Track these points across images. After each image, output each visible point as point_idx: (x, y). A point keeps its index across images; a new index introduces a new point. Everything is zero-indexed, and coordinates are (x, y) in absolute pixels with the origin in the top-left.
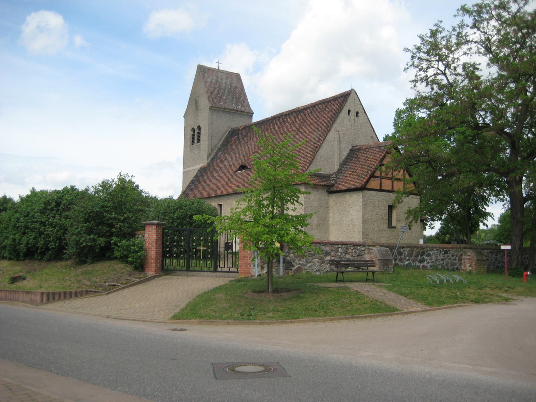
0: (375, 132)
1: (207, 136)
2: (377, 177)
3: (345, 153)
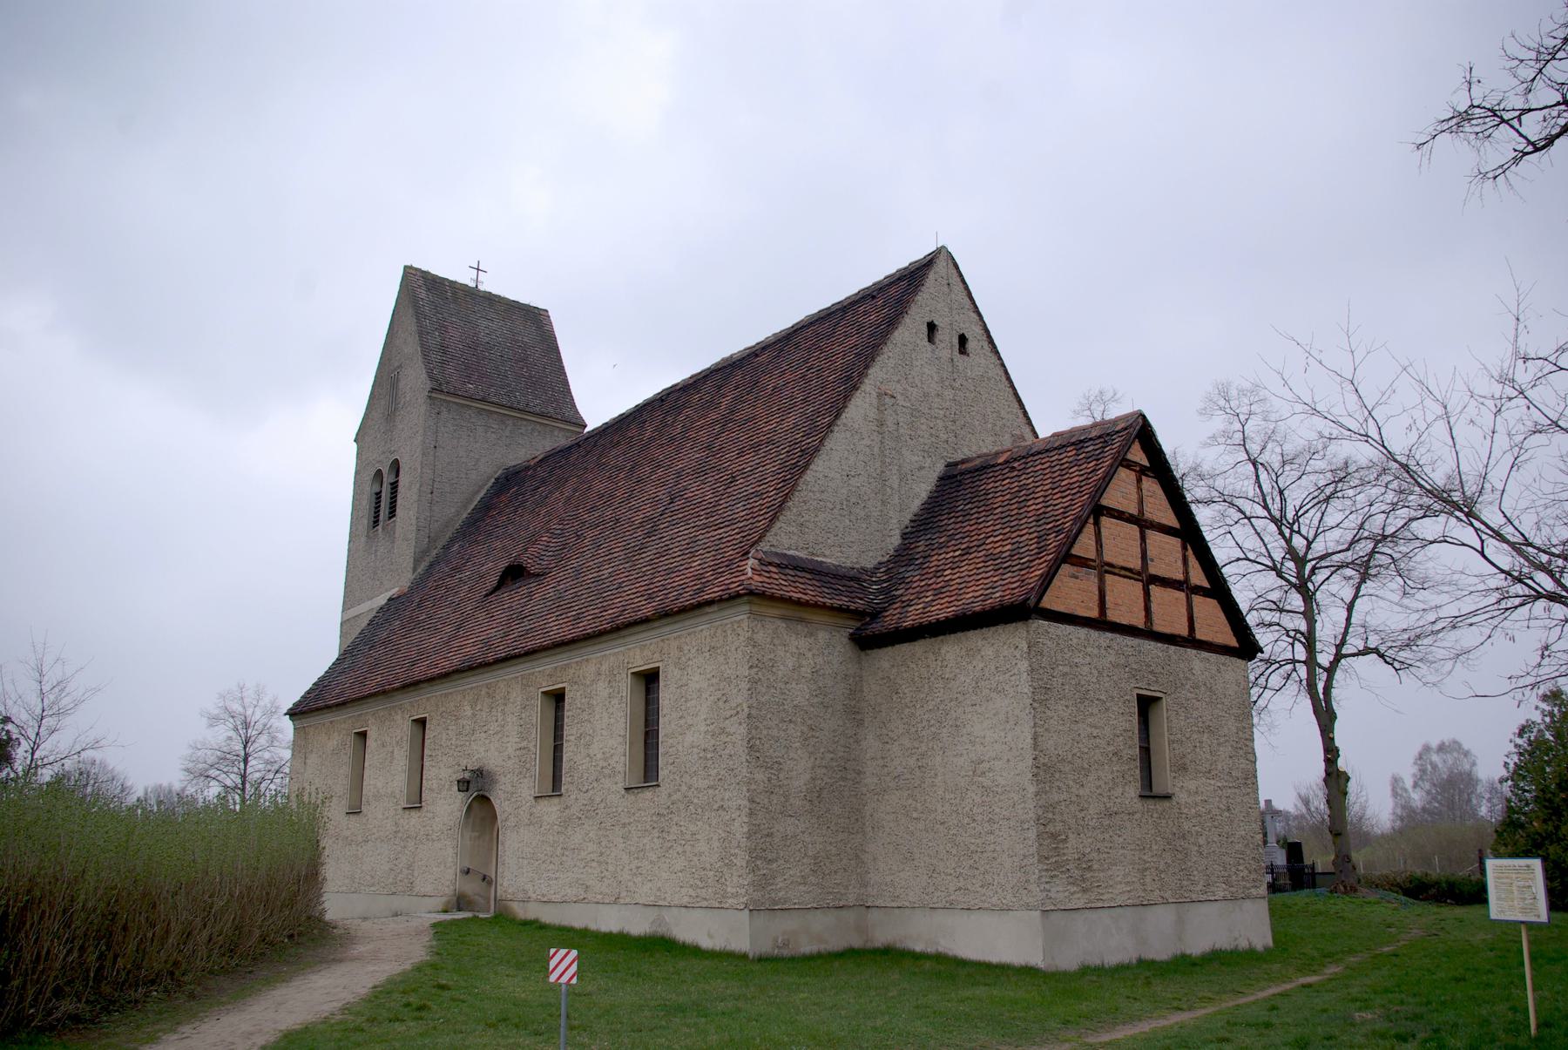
0: (1029, 423)
1: (415, 489)
2: (1082, 562)
3: (923, 489)
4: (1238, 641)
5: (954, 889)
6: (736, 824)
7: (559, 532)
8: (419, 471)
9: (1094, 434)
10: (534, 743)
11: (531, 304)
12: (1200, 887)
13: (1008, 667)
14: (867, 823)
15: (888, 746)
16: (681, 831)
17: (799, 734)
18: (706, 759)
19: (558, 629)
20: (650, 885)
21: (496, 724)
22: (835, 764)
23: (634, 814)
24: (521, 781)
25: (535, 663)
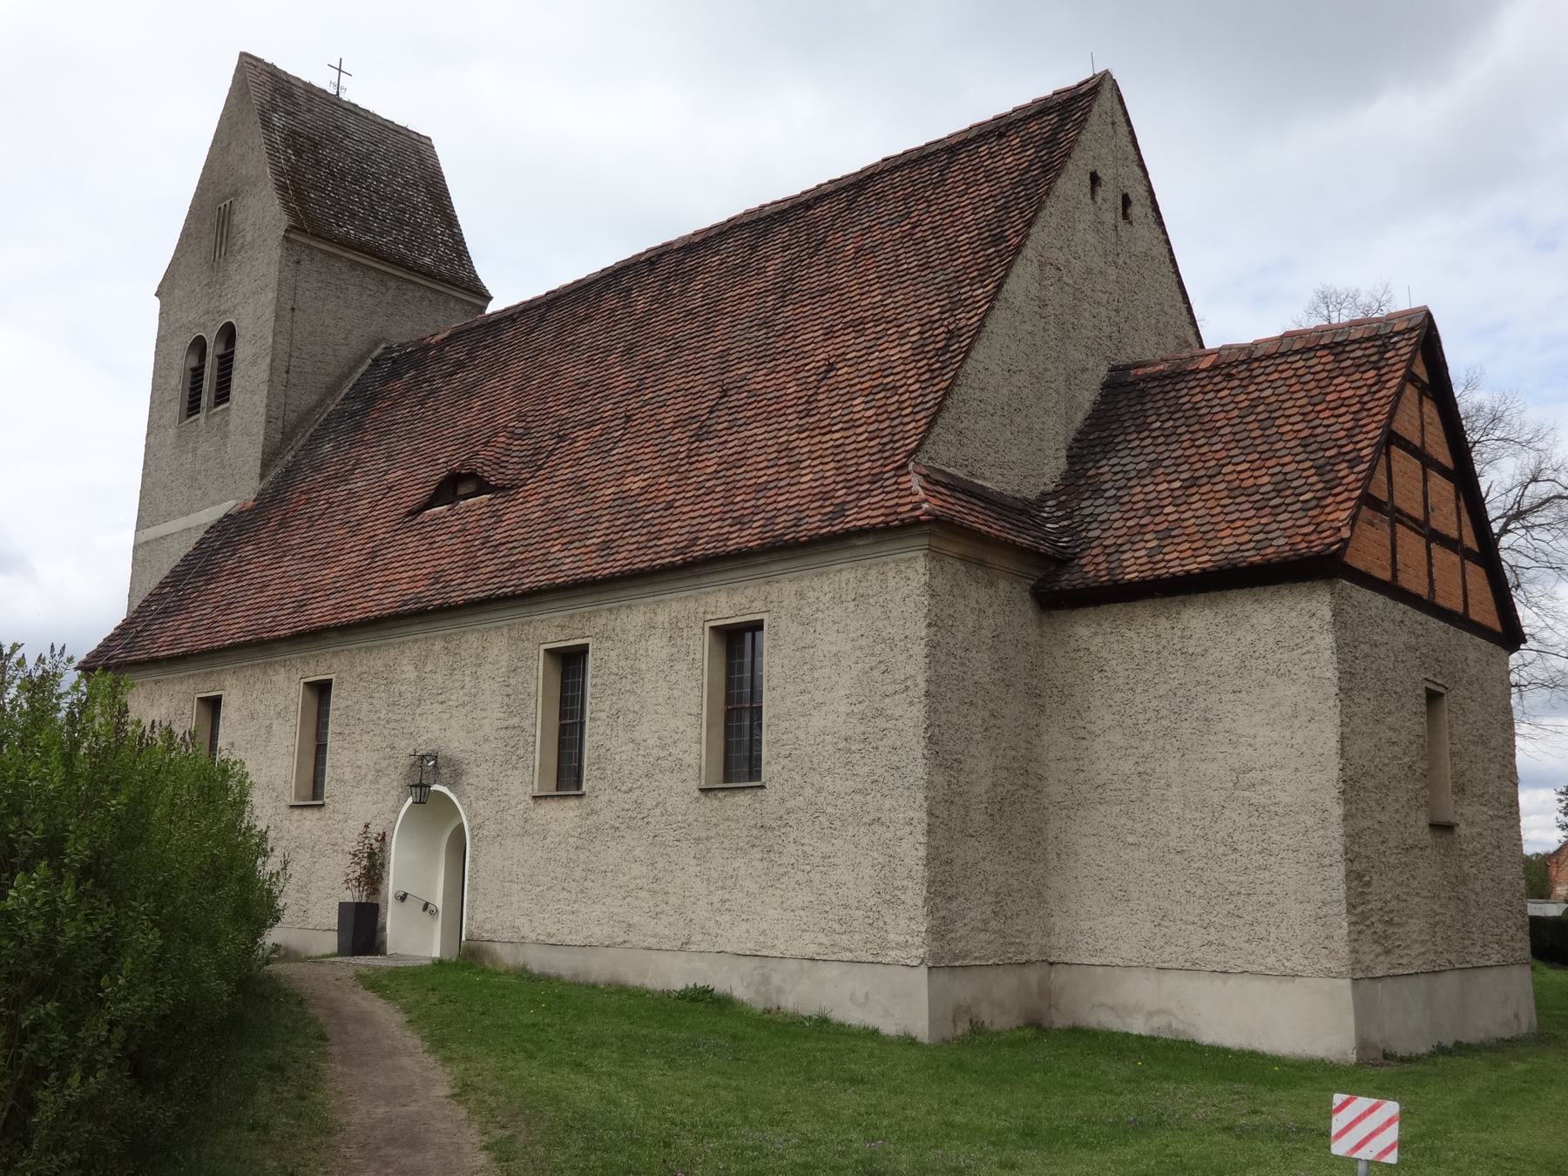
3: (1087, 397)
4: (1501, 624)
5: (1200, 943)
6: (905, 845)
7: (521, 431)
8: (271, 340)
9: (1356, 335)
10: (531, 721)
11: (410, 128)
12: (1477, 949)
13: (1297, 641)
14: (1049, 848)
15: (1085, 743)
16: (804, 852)
17: (980, 722)
18: (849, 750)
19: (570, 564)
20: (745, 926)
21: (461, 692)
22: (1016, 765)
23: (716, 825)
24: (509, 773)
25: (534, 609)
